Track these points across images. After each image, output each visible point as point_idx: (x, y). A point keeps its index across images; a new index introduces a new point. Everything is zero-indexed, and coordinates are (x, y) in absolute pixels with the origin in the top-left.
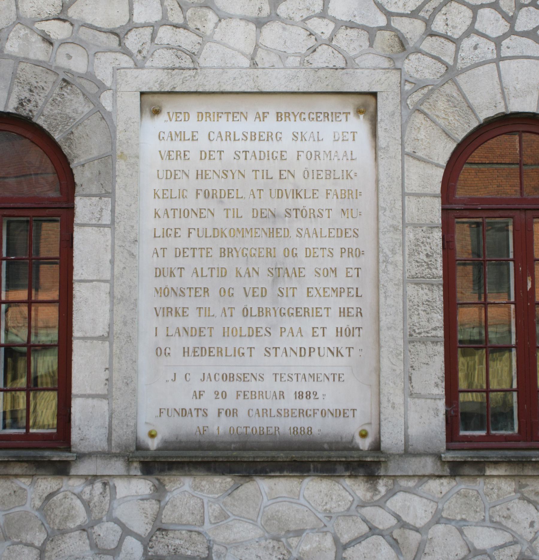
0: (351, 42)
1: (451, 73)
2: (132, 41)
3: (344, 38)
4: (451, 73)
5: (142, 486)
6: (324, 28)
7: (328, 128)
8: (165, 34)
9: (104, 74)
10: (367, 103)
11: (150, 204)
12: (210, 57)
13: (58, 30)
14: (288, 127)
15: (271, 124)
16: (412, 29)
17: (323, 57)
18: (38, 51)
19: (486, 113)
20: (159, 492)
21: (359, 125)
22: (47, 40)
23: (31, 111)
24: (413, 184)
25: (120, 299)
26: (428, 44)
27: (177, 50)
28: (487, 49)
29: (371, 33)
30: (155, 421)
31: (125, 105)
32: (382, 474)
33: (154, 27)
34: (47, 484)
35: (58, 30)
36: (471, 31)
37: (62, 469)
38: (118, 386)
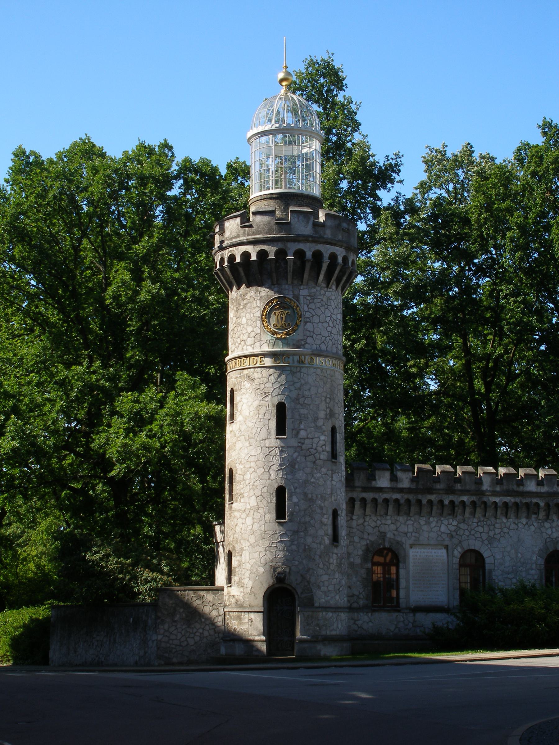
0: (444, 536)
1: (460, 542)
2: (409, 535)
3: (443, 535)
4: (460, 542)
5: (411, 615)
6: (440, 533)
7: (440, 551)
8: (413, 534)
9: (403, 541)
10: (447, 547)
11: (411, 565)
12: (421, 538)
13: (395, 532)
14: (433, 551)
15: (430, 550)
16: (454, 534)
17: (439, 538)
18: (392, 537)
19: (466, 549)
20: (414, 615)
21: (444, 551)
22: (394, 535)
23: (109, 426)
24: (454, 561)
25: (407, 581)
26: (457, 537)
27: (415, 537)
28: (466, 538)
29: (448, 534)
30: (413, 604)
31: (408, 546)
32: (343, 616)
33: (412, 533)
34: (396, 614)
35: (395, 532)
36: (464, 534)
37: (399, 611)
38: (408, 596)
